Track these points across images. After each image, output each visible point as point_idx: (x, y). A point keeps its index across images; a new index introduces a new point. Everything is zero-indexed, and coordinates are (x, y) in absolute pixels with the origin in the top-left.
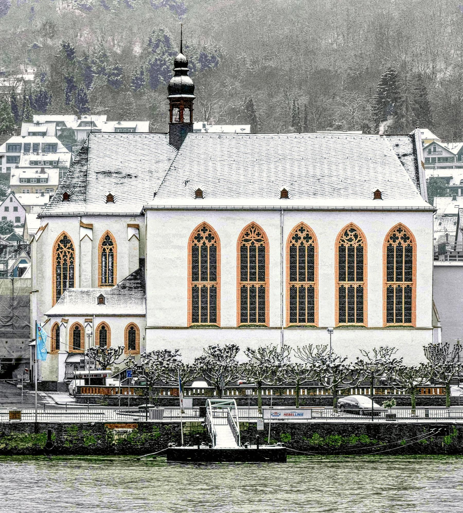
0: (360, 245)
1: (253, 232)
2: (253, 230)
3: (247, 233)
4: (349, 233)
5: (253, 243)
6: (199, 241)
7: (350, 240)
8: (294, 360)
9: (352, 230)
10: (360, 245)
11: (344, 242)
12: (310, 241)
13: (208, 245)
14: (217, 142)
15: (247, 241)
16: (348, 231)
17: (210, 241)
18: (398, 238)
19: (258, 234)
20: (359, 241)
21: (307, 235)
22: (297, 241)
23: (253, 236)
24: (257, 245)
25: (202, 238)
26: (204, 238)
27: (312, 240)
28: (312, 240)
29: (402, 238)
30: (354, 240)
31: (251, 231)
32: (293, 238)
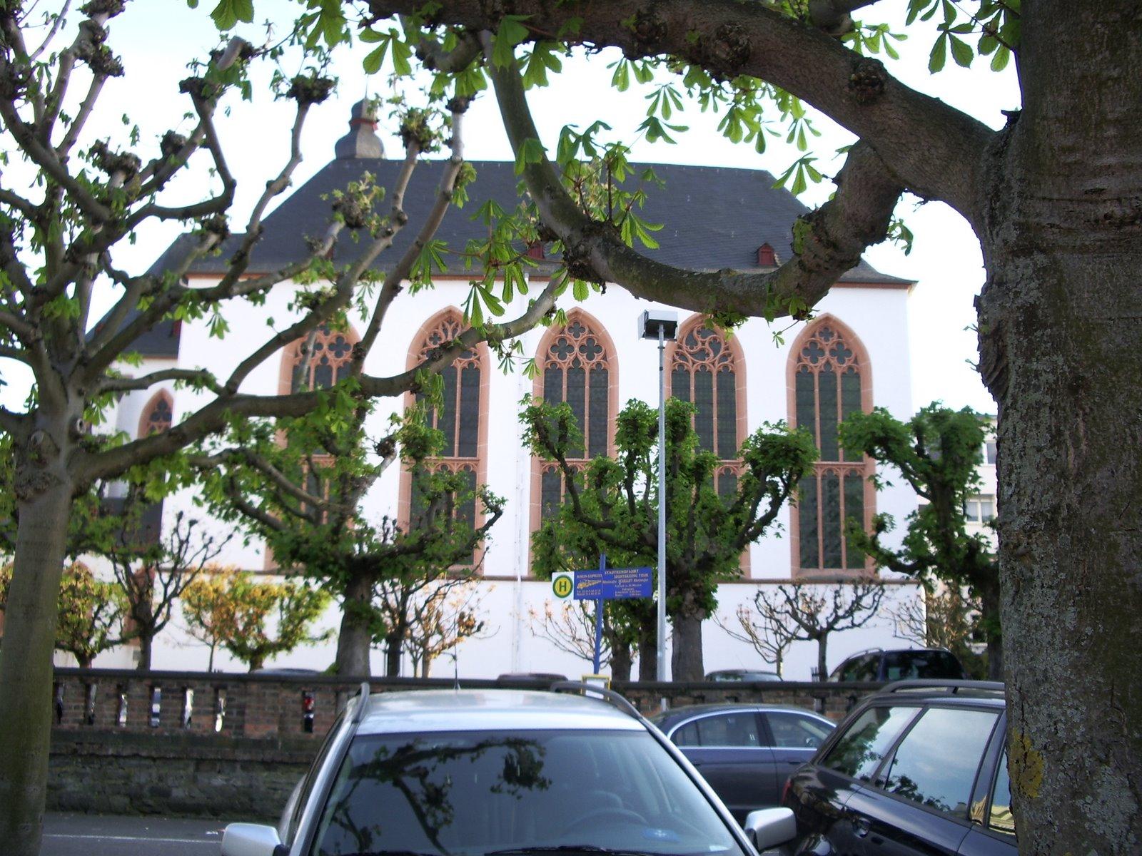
0: (726, 367)
7: (702, 354)
10: (726, 367)
13: (587, 365)
14: (260, 759)
16: (695, 333)
17: (841, 361)
20: (725, 357)
25: (822, 352)
28: (602, 354)
30: (712, 355)
32: (554, 347)
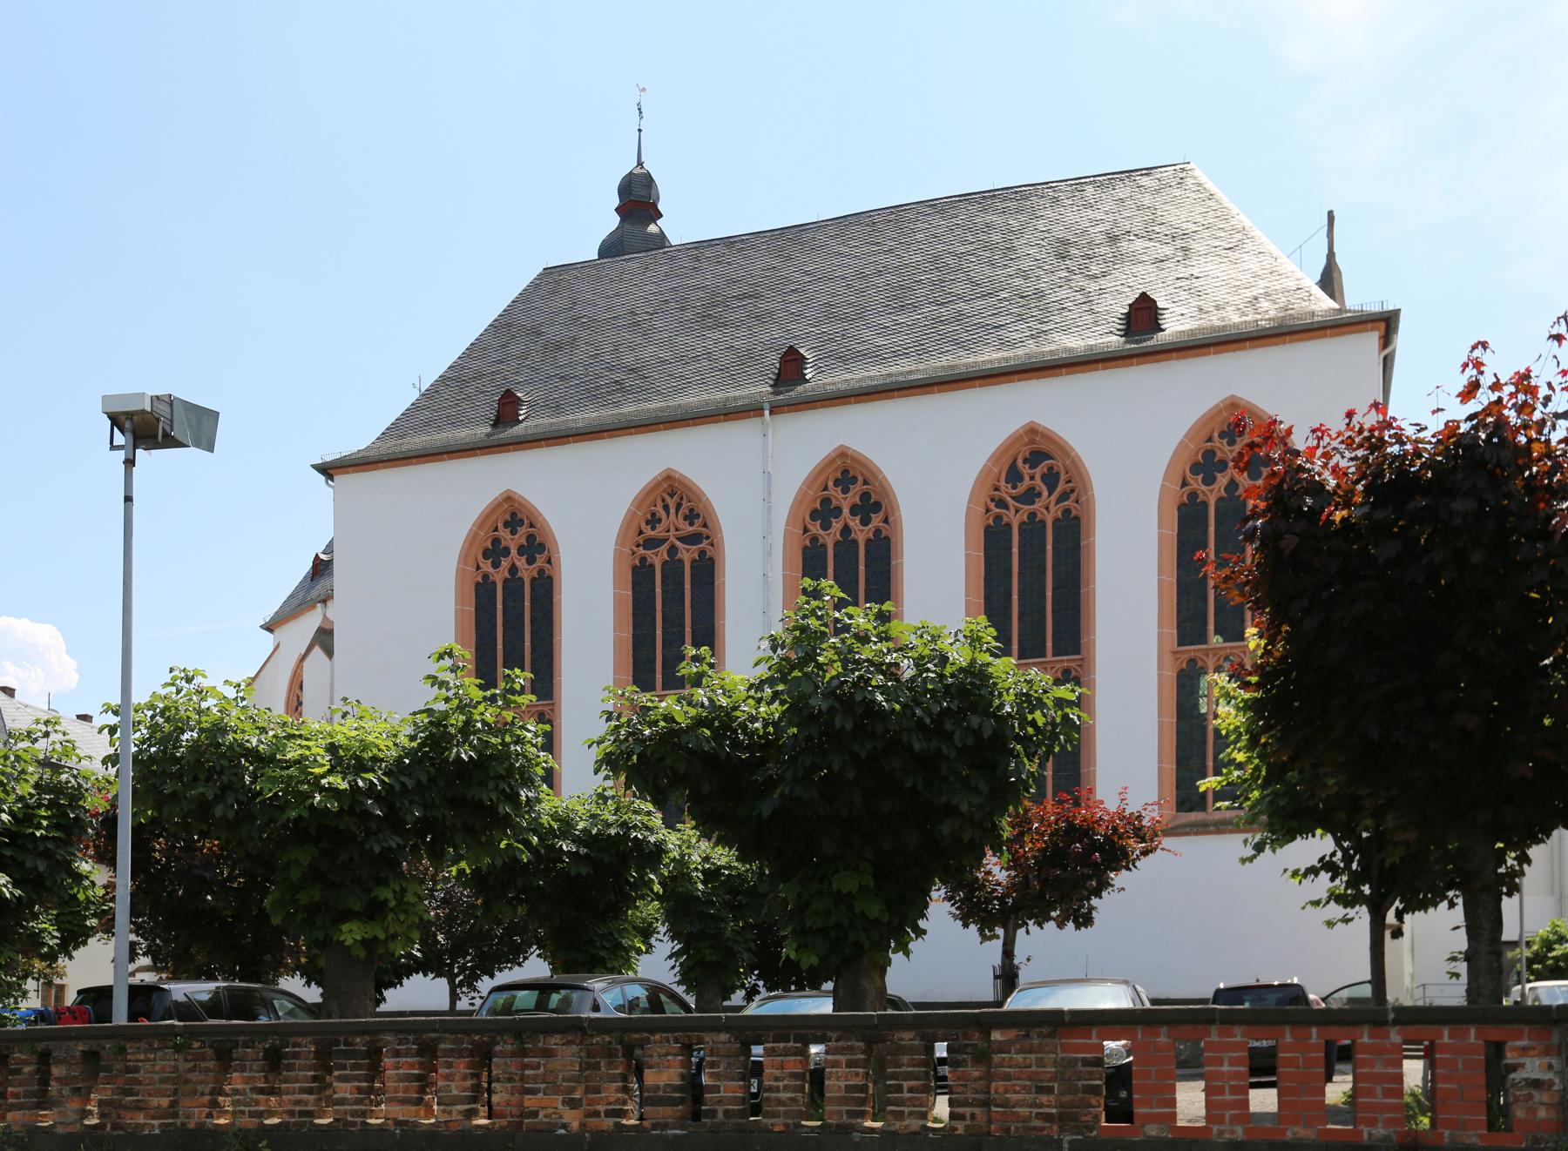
1: (672, 511)
2: (672, 503)
3: (854, 479)
4: (1039, 471)
5: (673, 550)
6: (826, 526)
7: (1030, 496)
8: (1545, 1001)
9: (1036, 457)
11: (1007, 508)
12: (876, 520)
13: (861, 534)
15: (651, 543)
18: (1223, 466)
19: (691, 517)
20: (1064, 497)
21: (531, 537)
22: (496, 565)
23: (674, 524)
24: (687, 554)
25: (854, 510)
26: (514, 552)
27: (881, 515)
29: (521, 550)
30: (1045, 493)
31: (666, 508)
